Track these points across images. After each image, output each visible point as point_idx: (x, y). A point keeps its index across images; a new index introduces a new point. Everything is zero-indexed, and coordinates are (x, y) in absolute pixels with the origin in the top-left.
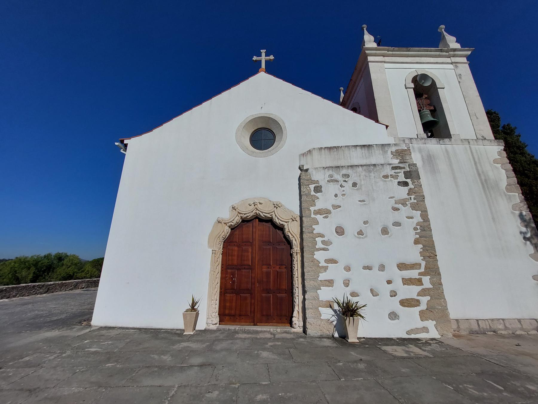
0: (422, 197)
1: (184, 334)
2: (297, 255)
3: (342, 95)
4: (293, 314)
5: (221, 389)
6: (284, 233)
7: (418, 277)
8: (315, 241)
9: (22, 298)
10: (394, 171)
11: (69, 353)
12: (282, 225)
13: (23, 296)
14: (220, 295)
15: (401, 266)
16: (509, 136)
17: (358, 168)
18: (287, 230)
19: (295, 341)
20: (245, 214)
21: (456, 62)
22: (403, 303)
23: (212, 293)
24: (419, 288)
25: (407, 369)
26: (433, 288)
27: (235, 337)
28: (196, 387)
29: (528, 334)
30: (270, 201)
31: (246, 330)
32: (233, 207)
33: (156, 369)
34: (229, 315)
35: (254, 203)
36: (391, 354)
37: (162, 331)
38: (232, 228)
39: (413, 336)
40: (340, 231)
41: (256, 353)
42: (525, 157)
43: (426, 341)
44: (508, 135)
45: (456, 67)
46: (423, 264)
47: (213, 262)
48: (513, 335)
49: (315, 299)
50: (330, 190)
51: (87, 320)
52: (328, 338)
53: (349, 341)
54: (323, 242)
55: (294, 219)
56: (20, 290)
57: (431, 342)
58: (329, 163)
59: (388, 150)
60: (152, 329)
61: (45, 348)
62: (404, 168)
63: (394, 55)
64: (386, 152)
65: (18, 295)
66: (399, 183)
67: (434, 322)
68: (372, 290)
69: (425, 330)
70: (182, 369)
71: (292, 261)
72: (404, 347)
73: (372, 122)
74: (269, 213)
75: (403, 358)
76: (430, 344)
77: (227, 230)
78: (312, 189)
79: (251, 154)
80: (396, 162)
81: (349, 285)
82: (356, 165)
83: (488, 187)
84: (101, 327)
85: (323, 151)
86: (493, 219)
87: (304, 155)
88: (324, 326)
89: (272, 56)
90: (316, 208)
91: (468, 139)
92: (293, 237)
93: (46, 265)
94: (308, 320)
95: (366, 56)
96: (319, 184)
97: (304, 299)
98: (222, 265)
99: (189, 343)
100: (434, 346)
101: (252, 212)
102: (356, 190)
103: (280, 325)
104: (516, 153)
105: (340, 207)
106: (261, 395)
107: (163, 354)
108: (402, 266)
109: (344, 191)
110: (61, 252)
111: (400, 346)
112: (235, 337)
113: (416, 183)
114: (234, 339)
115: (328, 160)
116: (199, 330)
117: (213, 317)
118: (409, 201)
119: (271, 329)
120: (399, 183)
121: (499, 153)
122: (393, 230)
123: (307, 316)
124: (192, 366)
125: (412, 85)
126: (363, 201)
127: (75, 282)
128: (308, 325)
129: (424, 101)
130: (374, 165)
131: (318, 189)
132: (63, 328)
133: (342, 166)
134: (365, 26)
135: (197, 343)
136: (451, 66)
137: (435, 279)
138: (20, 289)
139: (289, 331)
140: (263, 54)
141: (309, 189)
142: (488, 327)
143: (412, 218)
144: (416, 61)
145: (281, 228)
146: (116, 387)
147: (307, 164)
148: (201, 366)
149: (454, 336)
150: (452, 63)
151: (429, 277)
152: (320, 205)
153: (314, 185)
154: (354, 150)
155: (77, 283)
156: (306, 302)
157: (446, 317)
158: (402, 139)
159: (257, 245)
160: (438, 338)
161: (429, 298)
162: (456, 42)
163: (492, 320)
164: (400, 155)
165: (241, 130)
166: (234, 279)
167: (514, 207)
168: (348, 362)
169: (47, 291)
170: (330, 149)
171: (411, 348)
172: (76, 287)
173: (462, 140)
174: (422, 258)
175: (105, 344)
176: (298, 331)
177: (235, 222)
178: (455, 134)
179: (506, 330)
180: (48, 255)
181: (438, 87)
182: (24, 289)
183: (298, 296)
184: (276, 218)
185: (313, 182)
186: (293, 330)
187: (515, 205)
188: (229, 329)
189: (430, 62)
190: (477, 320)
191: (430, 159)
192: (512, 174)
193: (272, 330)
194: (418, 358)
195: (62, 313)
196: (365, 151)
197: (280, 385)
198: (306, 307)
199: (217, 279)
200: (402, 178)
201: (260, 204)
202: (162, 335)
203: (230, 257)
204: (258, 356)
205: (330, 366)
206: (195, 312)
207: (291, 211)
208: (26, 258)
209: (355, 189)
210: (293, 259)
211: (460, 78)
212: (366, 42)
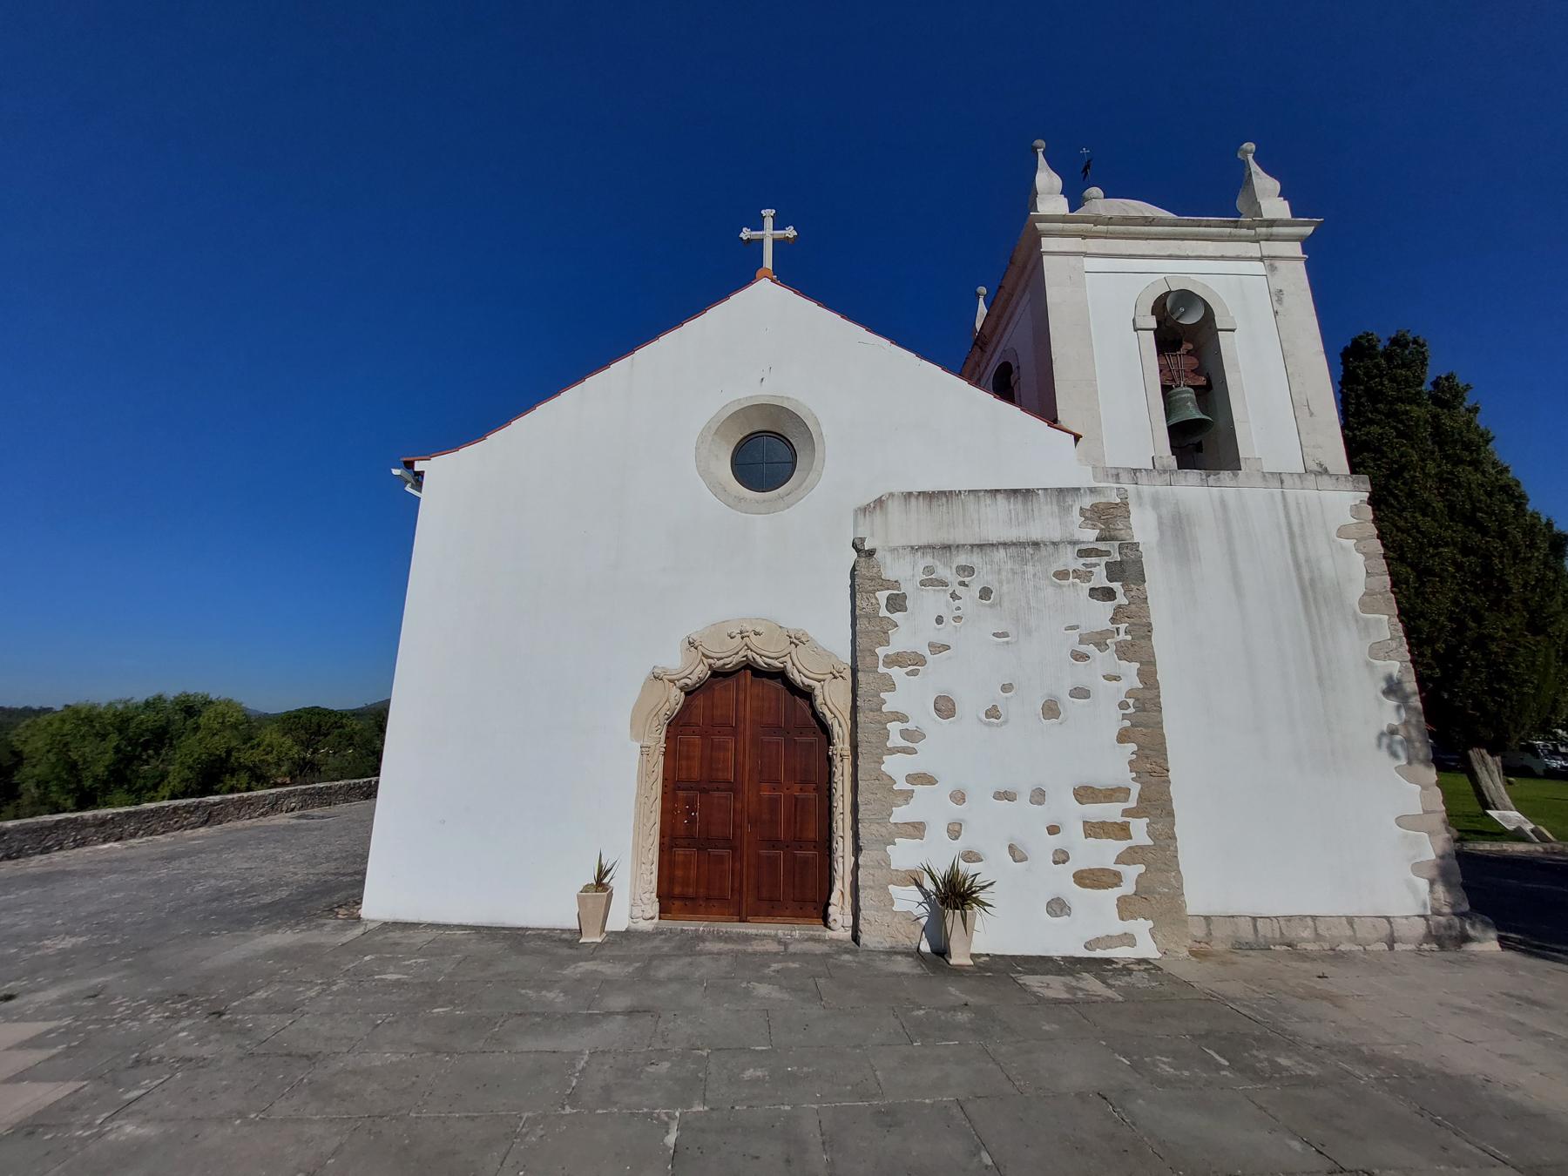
0: (1146, 629)
1: (581, 941)
2: (842, 761)
3: (982, 309)
4: (829, 898)
5: (674, 1058)
6: (812, 706)
7: (1120, 819)
9: (150, 838)
10: (1082, 561)
11: (342, 984)
13: (151, 835)
14: (661, 850)
15: (1082, 792)
16: (1445, 411)
18: (819, 701)
19: (831, 960)
20: (719, 659)
21: (1273, 254)
22: (1082, 878)
23: (643, 847)
24: (1122, 845)
25: (1054, 1026)
26: (1154, 845)
27: (698, 948)
28: (626, 1054)
29: (1365, 949)
30: (780, 627)
31: (722, 931)
32: (689, 642)
33: (538, 1019)
34: (683, 898)
35: (741, 633)
36: (1034, 994)
38: (687, 690)
39: (1099, 953)
40: (945, 707)
41: (745, 988)
42: (1483, 473)
43: (1124, 965)
44: (1442, 408)
45: (1273, 268)
46: (1135, 789)
47: (643, 775)
48: (1331, 953)
49: (880, 866)
50: (924, 605)
51: (345, 905)
52: (907, 954)
53: (951, 962)
54: (905, 734)
55: (837, 675)
56: (144, 819)
57: (1135, 967)
59: (1072, 506)
60: (504, 928)
61: (285, 971)
62: (1108, 553)
63: (1111, 233)
64: (1068, 510)
65: (141, 832)
66: (1093, 592)
67: (1150, 924)
68: (1011, 847)
69: (1128, 939)
70: (591, 1020)
71: (831, 774)
72: (1070, 978)
73: (1038, 425)
74: (777, 659)
75: (1057, 1002)
76: (1130, 972)
77: (676, 697)
78: (883, 602)
79: (735, 503)
80: (1089, 535)
81: (959, 836)
83: (1315, 599)
84: (386, 923)
85: (913, 500)
86: (1320, 679)
87: (867, 512)
88: (899, 926)
89: (792, 228)
90: (890, 650)
91: (1280, 473)
92: (835, 717)
93: (150, 728)
94: (863, 913)
95: (1037, 238)
96: (899, 589)
97: (856, 866)
98: (665, 780)
99: (595, 962)
100: (1140, 979)
101: (737, 653)
103: (801, 920)
104: (1459, 461)
105: (948, 648)
106: (752, 1070)
108: (1085, 794)
109: (958, 608)
110: (191, 691)
111: (1062, 975)
112: (698, 948)
113: (1133, 594)
114: (694, 955)
115: (922, 526)
116: (612, 932)
117: (646, 901)
118: (1113, 638)
119: (780, 931)
120: (1093, 592)
121: (1355, 510)
122: (1071, 706)
123: (861, 904)
124: (609, 1014)
125: (1152, 322)
126: (1004, 635)
127: (273, 794)
128: (863, 925)
129: (1183, 361)
130: (1036, 544)
131: (897, 603)
132: (298, 924)
133: (958, 546)
134: (1040, 144)
135: (614, 963)
136: (1259, 267)
137: (1159, 826)
138: (144, 816)
139: (819, 935)
140: (769, 223)
141: (874, 601)
142: (1278, 935)
143: (1117, 678)
144: (1168, 253)
145: (807, 695)
146: (469, 1052)
147: (872, 535)
148: (631, 1013)
149: (1193, 953)
150: (1261, 259)
151: (1147, 820)
152: (900, 641)
153: (887, 593)
154: (988, 501)
155: (278, 797)
156: (859, 874)
157: (1176, 912)
158: (1114, 472)
159: (748, 733)
160: (1155, 959)
161: (1141, 868)
162: (1279, 196)
163: (1289, 918)
164: (1103, 517)
165: (710, 438)
167: (1377, 651)
168: (937, 1009)
169: (207, 821)
170: (930, 496)
171: (1084, 980)
172: (274, 806)
173: (1264, 476)
174: (1134, 775)
175: (411, 965)
176: (841, 938)
177: (694, 678)
178: (1249, 459)
179: (1319, 941)
180: (155, 699)
181: (1218, 327)
182: (153, 816)
183: (843, 857)
184: (795, 671)
186: (829, 934)
187: (1377, 645)
188: (682, 930)
189: (1203, 254)
190: (1254, 919)
191: (1177, 527)
192: (1382, 565)
193: (780, 933)
194: (1091, 1001)
195: (275, 884)
196: (1017, 505)
197: (791, 1053)
198: (859, 883)
199: (654, 813)
200: (1100, 579)
201: (757, 634)
202: (532, 944)
203: (684, 763)
204: (747, 993)
205: (897, 1017)
206: (605, 894)
207: (830, 655)
208: (93, 707)
210: (834, 769)
211: (1280, 301)
212: (1042, 193)
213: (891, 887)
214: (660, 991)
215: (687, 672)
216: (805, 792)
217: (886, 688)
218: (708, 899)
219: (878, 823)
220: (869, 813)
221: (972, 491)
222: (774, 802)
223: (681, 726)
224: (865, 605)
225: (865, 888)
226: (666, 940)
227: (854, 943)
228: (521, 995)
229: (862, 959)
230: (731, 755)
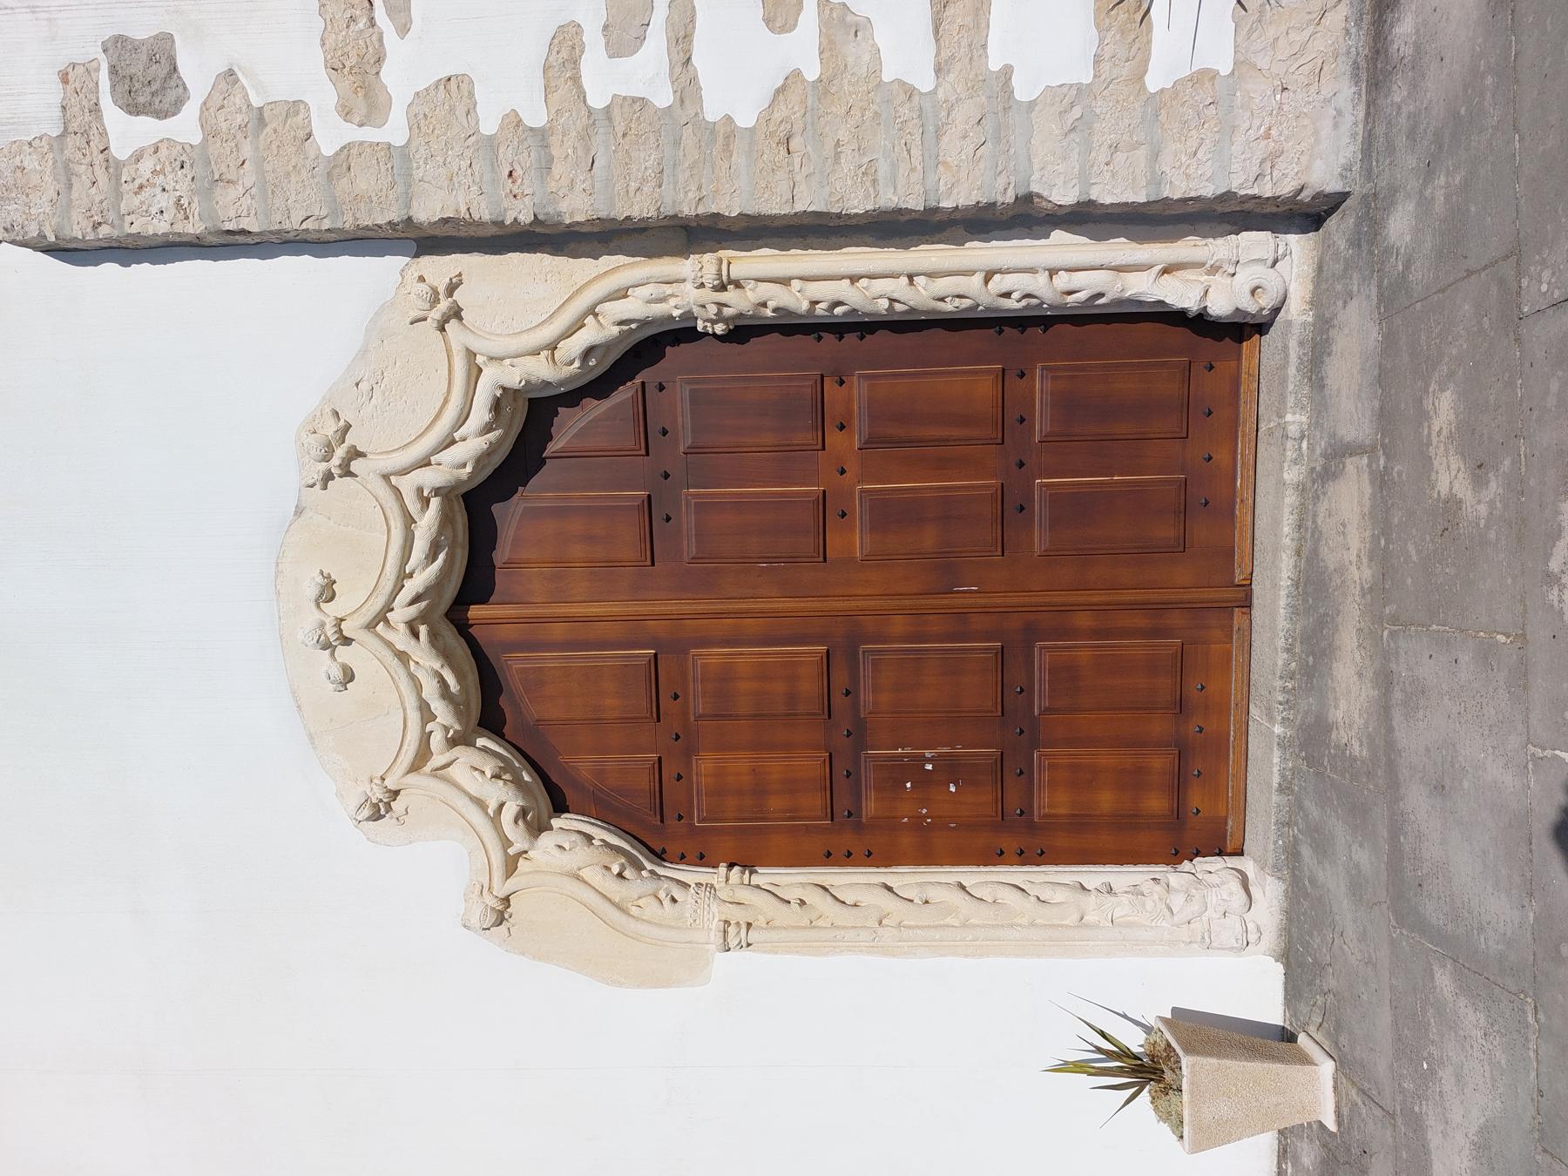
2: (738, 284)
6: (573, 396)
14: (1041, 857)
18: (541, 370)
20: (427, 714)
34: (1178, 785)
35: (326, 645)
55: (444, 304)
71: (791, 327)
74: (409, 521)
78: (146, 129)
96: (90, 69)
98: (828, 858)
101: (403, 657)
103: (1245, 411)
114: (1391, 768)
139: (1301, 344)
141: (146, 166)
153: (113, 115)
159: (672, 607)
177: (499, 793)
183: (1052, 272)
186: (1297, 311)
188: (1281, 790)
193: (1292, 475)
201: (328, 592)
203: (775, 803)
206: (1186, 1061)
210: (769, 313)
213: (1155, 81)
216: (850, 413)
217: (460, 111)
218: (1181, 706)
219: (938, 135)
224: (164, 201)
225: (1156, 180)
226: (1323, 847)
227: (1332, 223)
229: (1410, 161)
230: (747, 656)
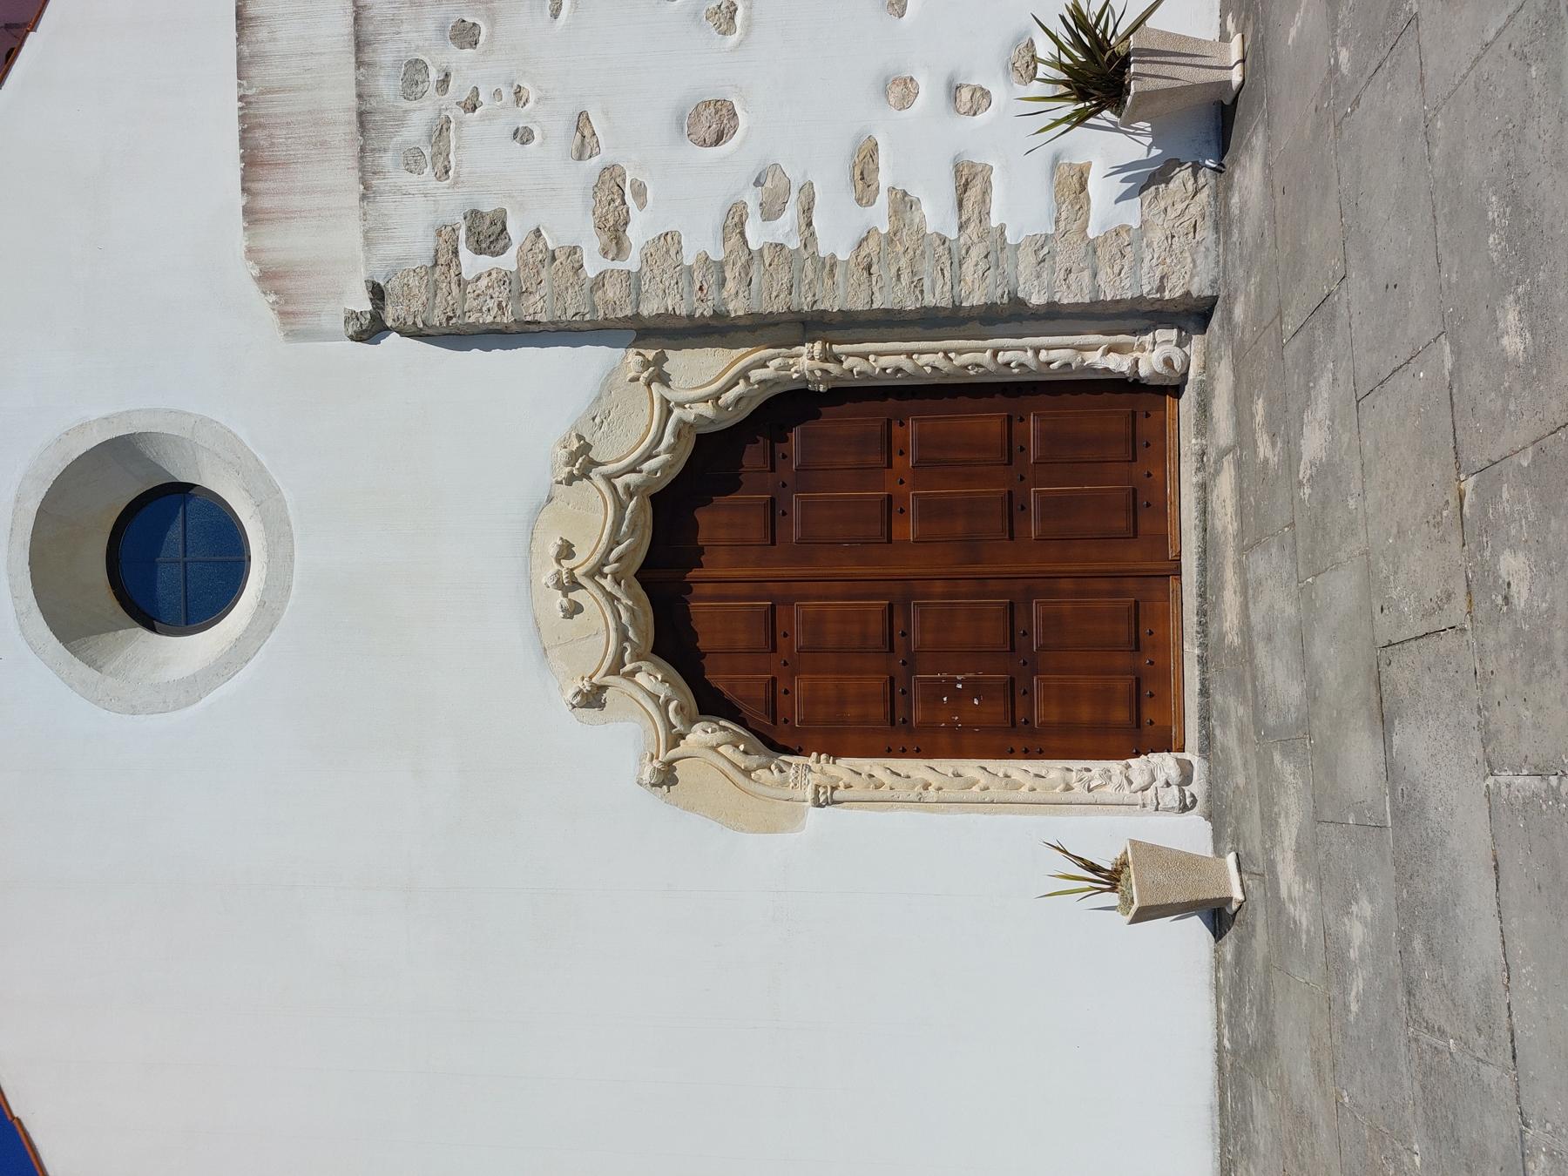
8: (766, 252)
12: (678, 434)
17: (372, 13)
30: (550, 500)
33: (1418, 944)
34: (1137, 700)
37: (1231, 1040)
54: (770, 212)
58: (341, 174)
60: (1222, 1105)
70: (1408, 808)
78: (486, 262)
82: (356, 19)
85: (265, 203)
87: (289, 308)
98: (889, 753)
102: (493, 26)
105: (583, 119)
107: (1342, 958)
124: (1391, 770)
133: (360, 96)
141: (483, 283)
148: (1384, 721)
153: (465, 254)
154: (263, 34)
159: (786, 571)
165: (110, 680)
166: (960, 686)
170: (252, 162)
185: (444, 259)
203: (852, 711)
204: (1325, 471)
209: (491, 36)
214: (1331, 675)
215: (651, 707)
217: (673, 252)
220: (940, 283)
221: (238, 72)
222: (929, 510)
223: (774, 722)
228: (1362, 1010)
